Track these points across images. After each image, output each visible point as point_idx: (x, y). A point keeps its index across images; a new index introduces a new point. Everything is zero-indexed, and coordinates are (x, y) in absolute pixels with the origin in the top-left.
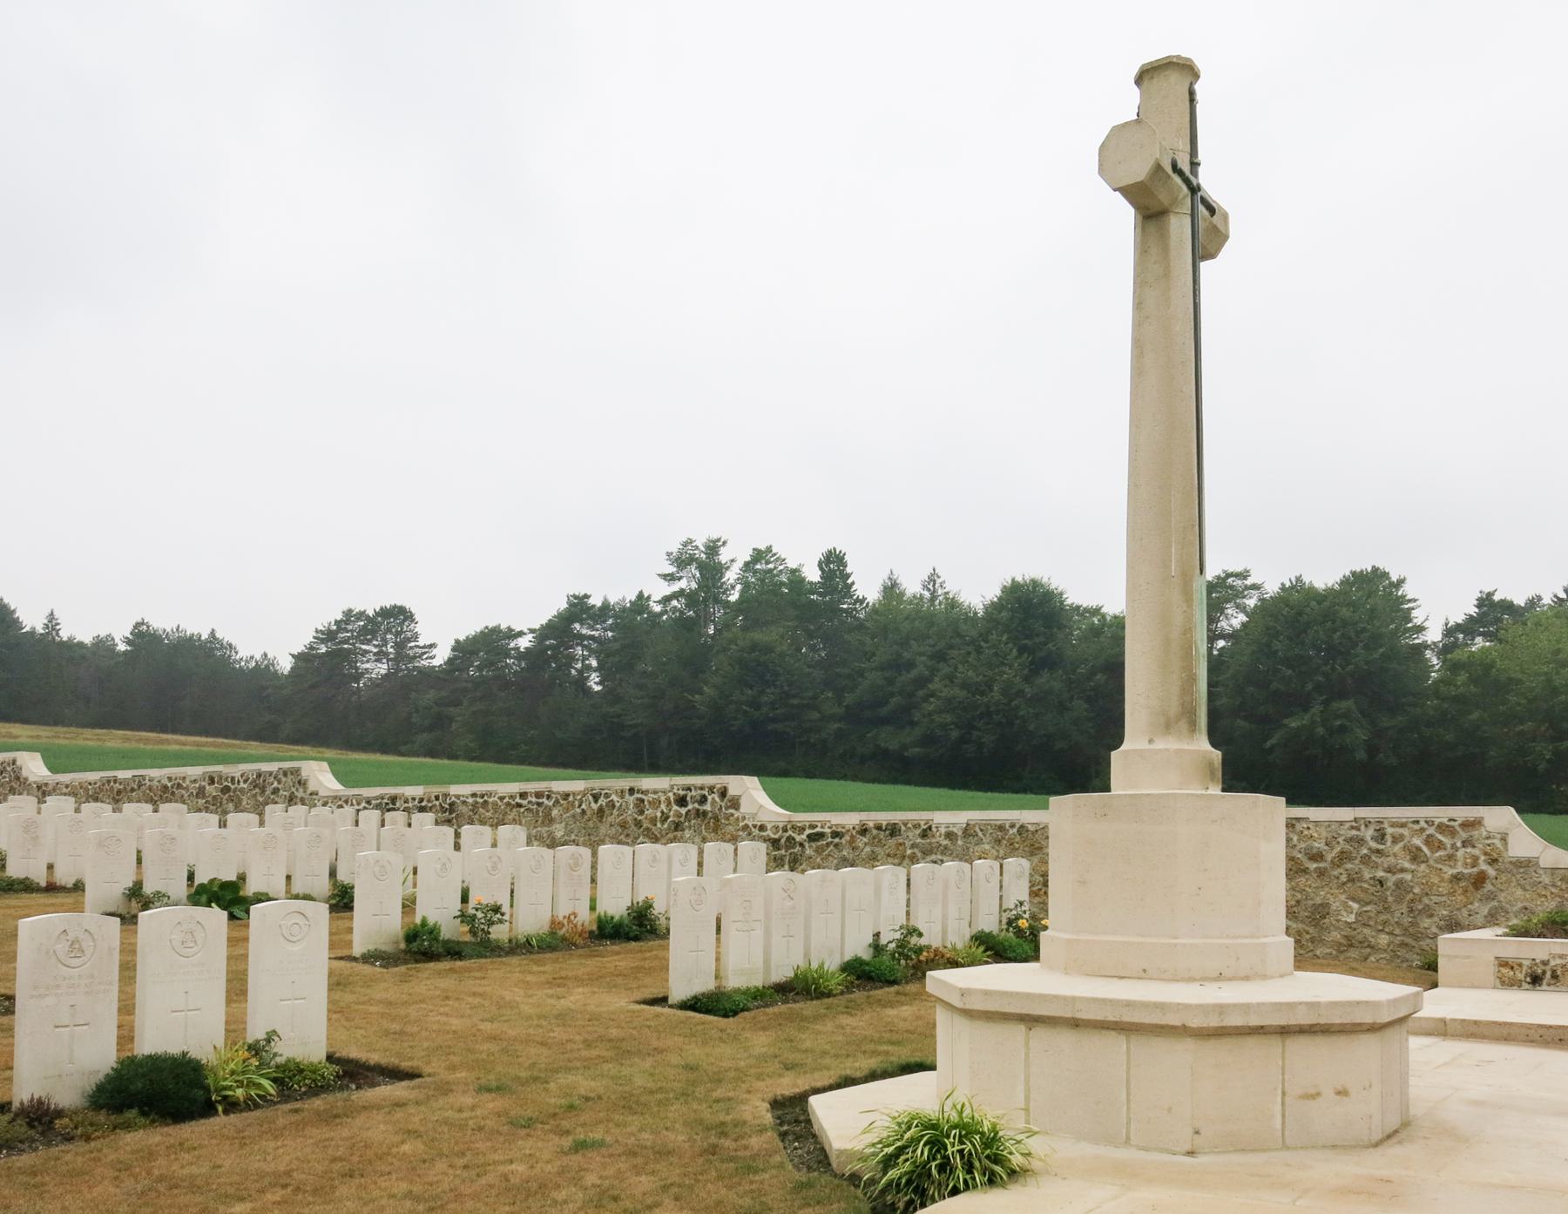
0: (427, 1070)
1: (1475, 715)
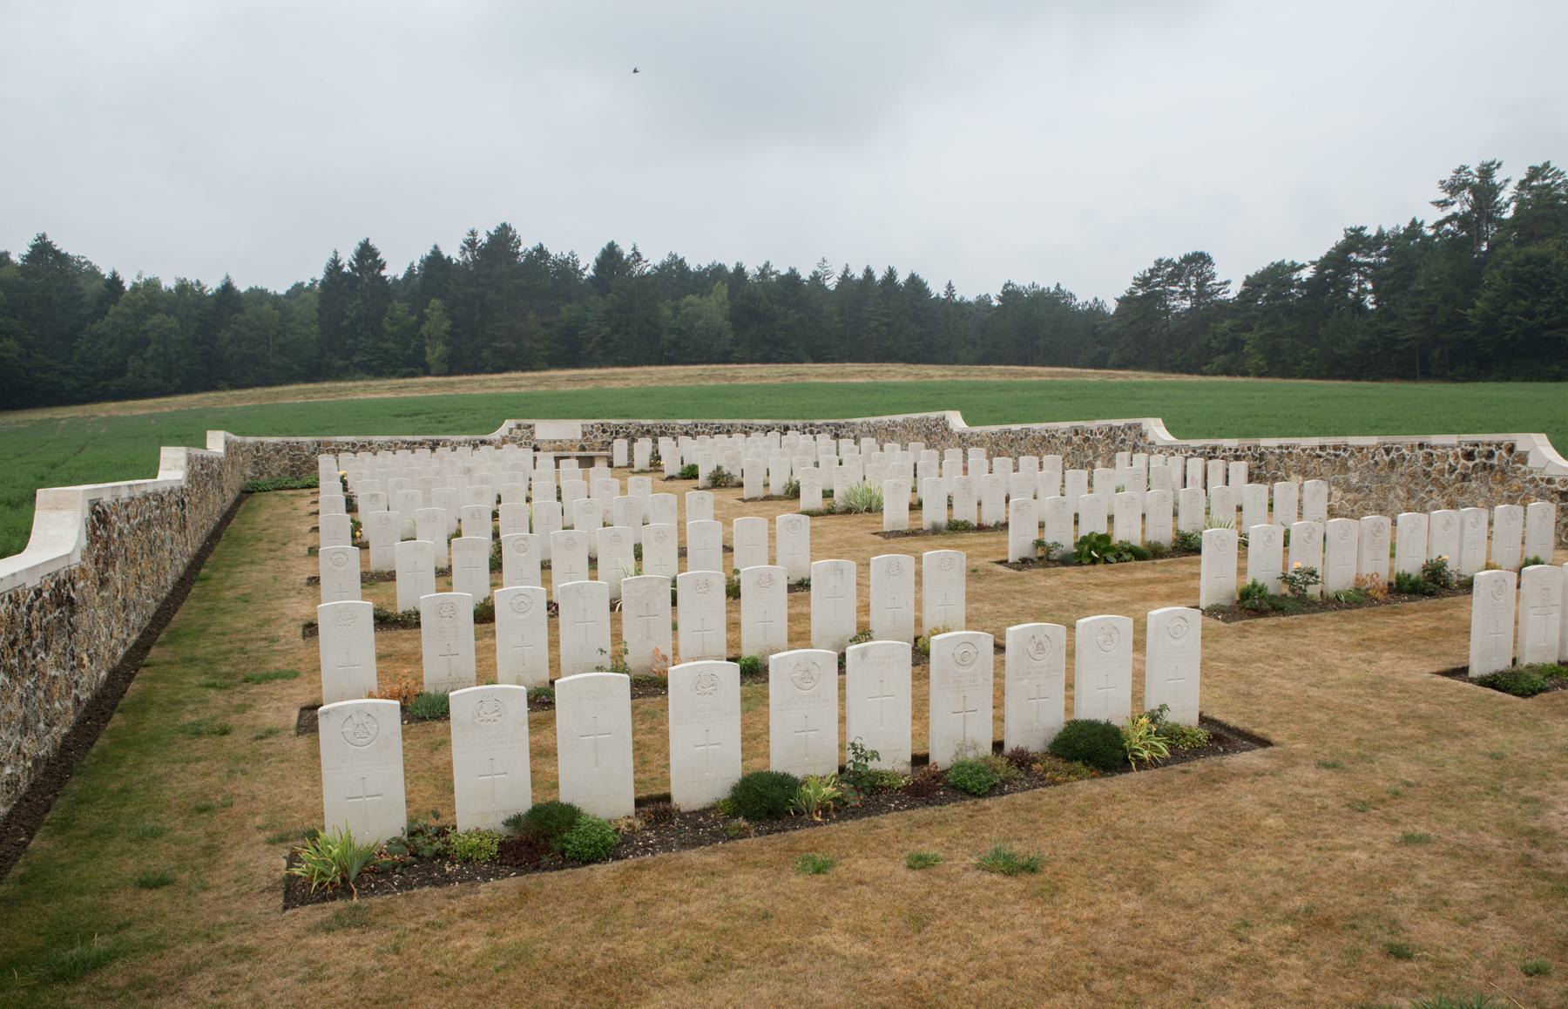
0: (1274, 738)
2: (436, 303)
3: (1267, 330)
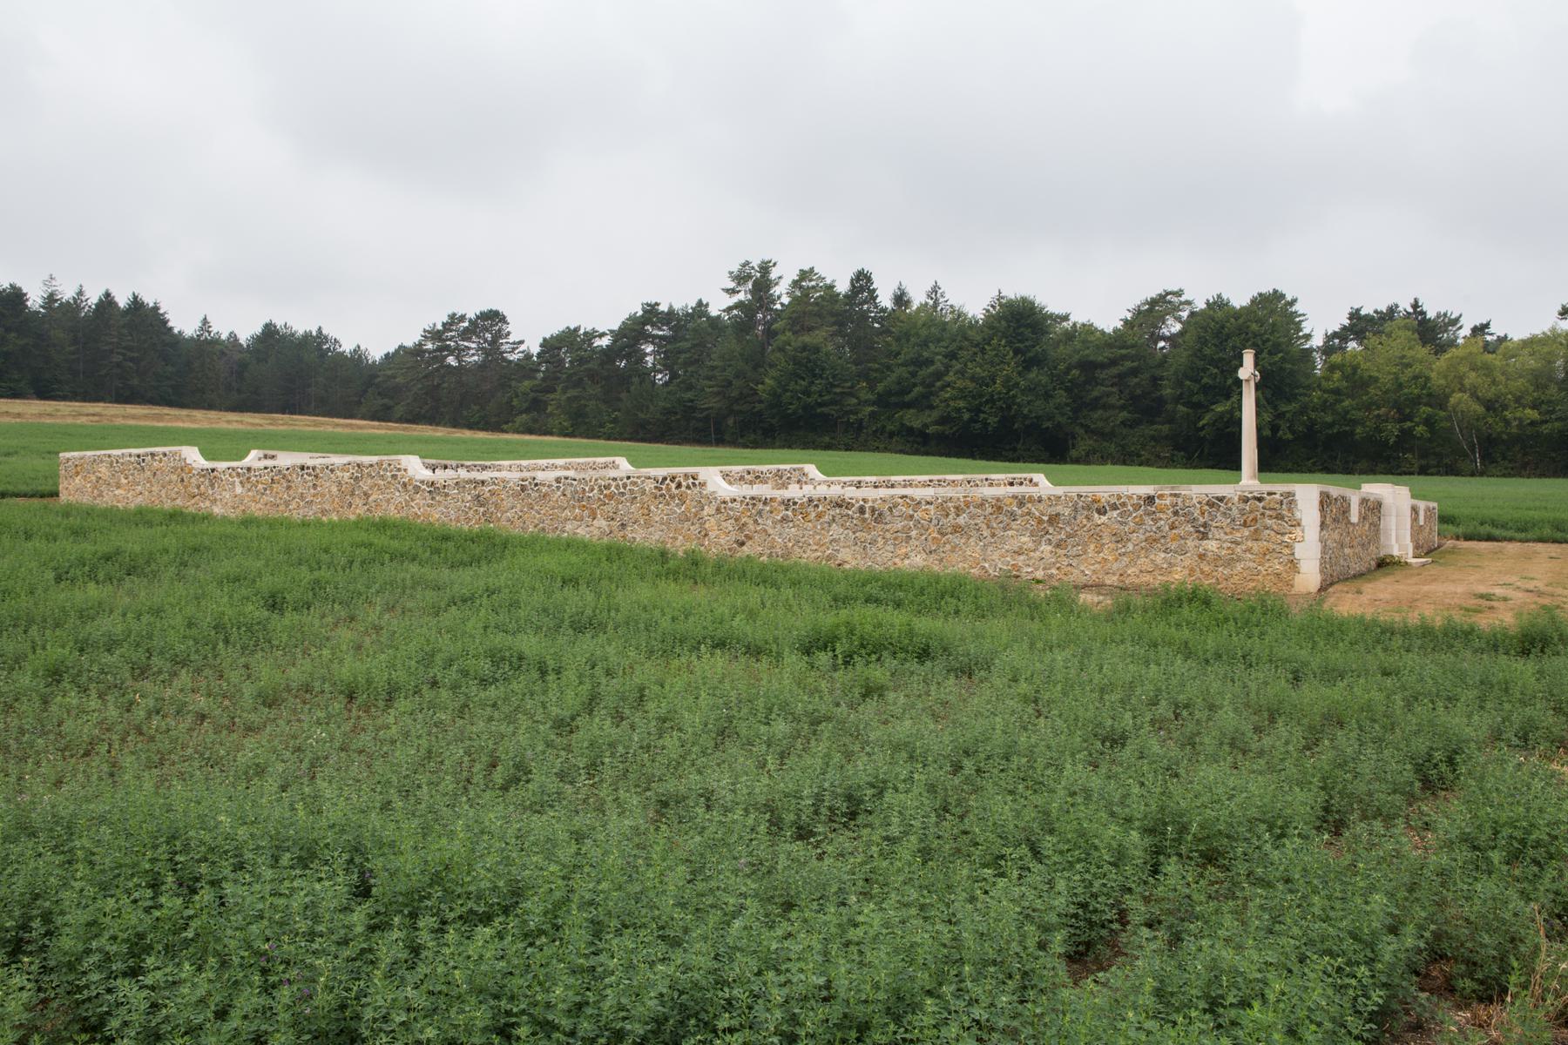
1: (1346, 403)
3: (572, 393)
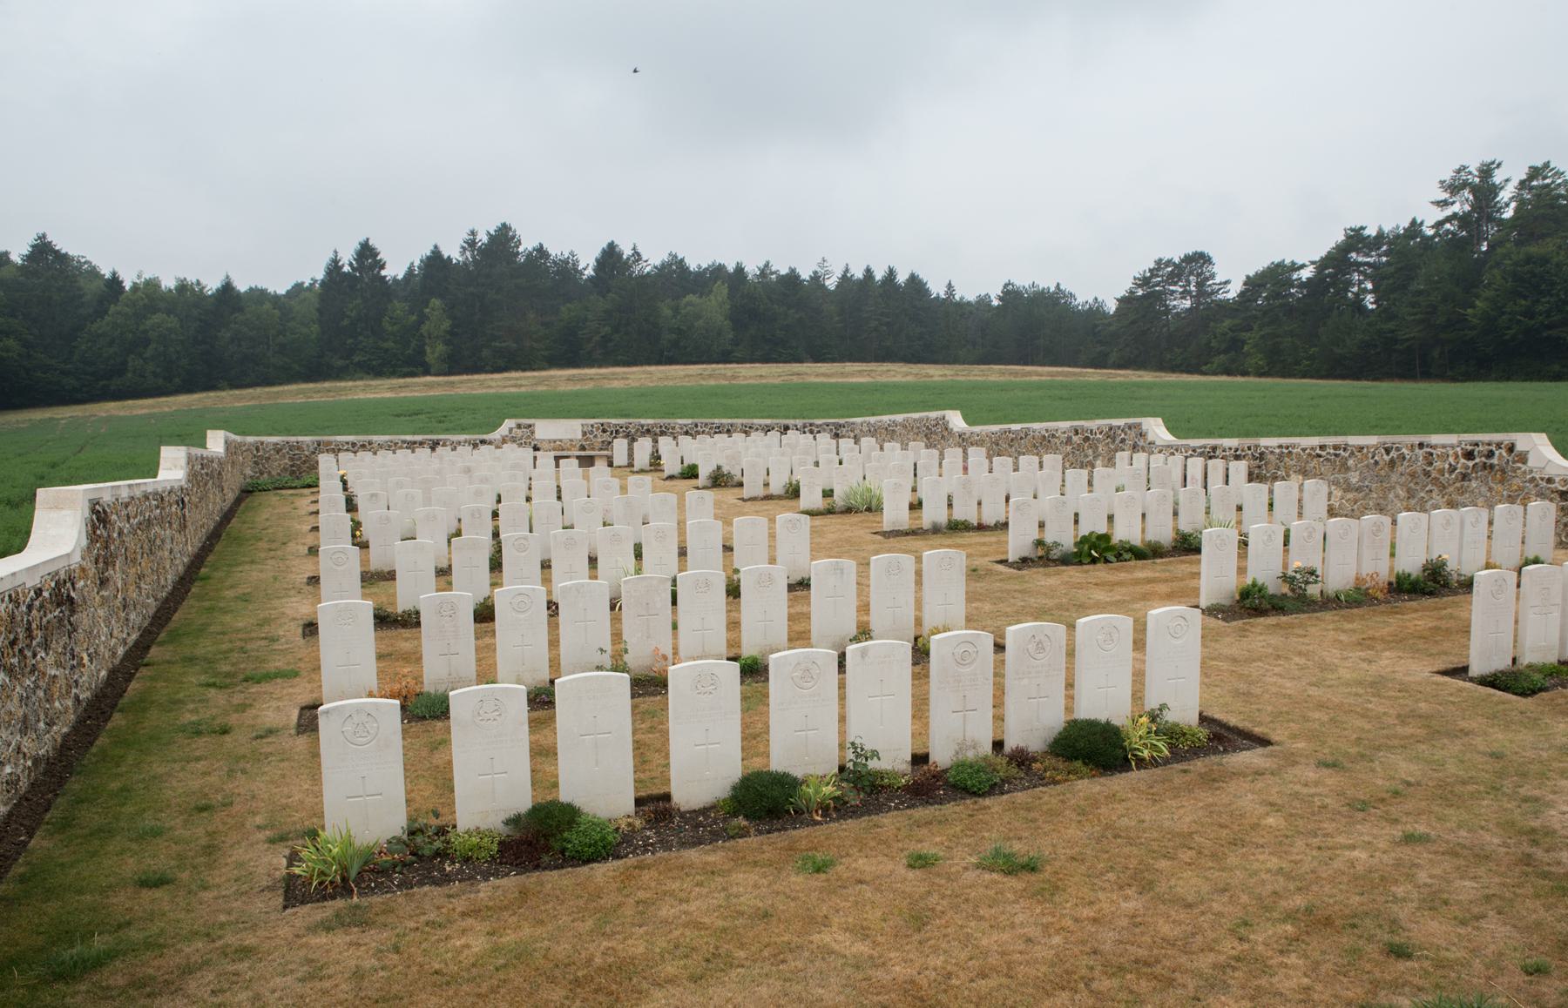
0: (1274, 737)
2: (436, 302)
3: (1267, 330)
